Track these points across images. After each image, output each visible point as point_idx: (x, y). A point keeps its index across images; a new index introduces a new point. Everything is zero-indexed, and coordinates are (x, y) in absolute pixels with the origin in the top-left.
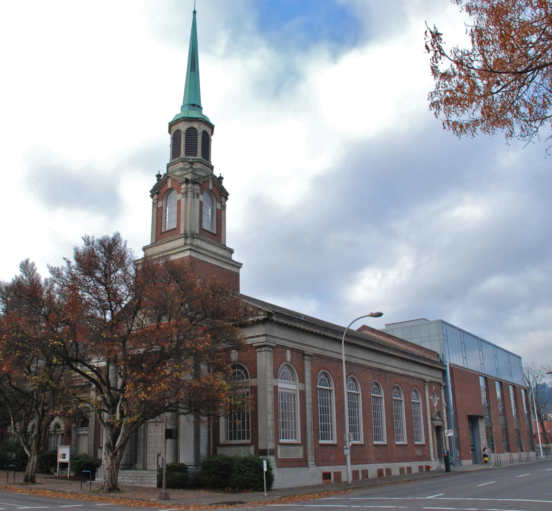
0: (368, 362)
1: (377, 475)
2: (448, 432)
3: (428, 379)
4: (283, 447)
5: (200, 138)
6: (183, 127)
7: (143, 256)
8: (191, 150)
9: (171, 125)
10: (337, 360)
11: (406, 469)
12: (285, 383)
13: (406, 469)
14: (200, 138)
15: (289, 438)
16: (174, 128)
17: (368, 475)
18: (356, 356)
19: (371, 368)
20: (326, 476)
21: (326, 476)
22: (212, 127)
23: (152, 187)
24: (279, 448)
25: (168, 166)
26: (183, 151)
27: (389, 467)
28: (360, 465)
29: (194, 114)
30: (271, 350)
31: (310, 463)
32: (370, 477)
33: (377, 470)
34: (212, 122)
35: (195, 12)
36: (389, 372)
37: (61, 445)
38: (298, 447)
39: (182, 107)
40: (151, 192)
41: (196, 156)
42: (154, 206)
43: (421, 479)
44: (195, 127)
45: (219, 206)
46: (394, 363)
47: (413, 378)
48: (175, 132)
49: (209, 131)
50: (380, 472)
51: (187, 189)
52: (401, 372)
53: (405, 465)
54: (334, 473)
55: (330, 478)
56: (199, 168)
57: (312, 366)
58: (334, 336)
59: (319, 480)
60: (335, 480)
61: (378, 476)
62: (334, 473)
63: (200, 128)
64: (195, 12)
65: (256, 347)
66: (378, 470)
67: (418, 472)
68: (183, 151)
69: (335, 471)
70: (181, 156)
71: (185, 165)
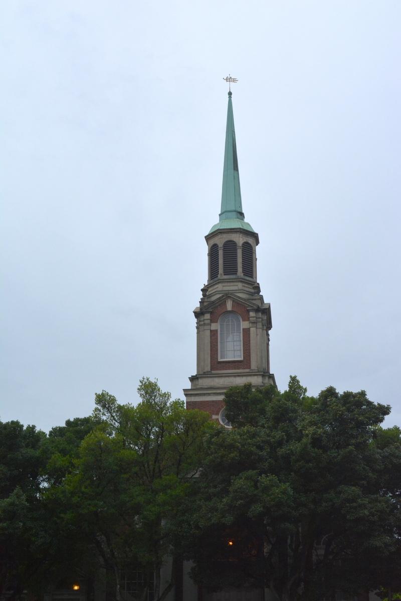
6: (220, 241)
7: (195, 375)
8: (230, 268)
9: (208, 238)
16: (212, 242)
22: (255, 236)
23: (83, 417)
26: (221, 271)
29: (235, 224)
34: (256, 231)
35: (230, 94)
37: (252, 277)
39: (220, 215)
40: (363, 394)
41: (236, 274)
42: (202, 328)
44: (249, 242)
45: (265, 318)
48: (212, 247)
49: (251, 241)
56: (240, 288)
63: (240, 240)
64: (230, 94)
68: (221, 271)
70: (219, 276)
71: (223, 286)
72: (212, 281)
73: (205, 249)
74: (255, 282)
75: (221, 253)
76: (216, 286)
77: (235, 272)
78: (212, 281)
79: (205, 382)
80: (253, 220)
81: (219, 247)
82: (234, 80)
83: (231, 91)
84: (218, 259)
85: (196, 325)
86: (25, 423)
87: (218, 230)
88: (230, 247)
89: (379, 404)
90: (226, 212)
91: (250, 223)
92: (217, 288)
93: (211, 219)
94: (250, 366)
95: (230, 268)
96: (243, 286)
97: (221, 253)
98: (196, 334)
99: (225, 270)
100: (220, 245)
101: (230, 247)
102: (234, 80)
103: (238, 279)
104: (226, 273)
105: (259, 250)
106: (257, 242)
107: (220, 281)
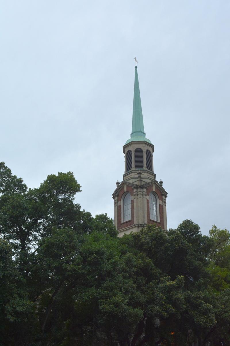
5: (145, 155)
6: (133, 148)
8: (139, 165)
9: (125, 147)
14: (145, 155)
22: (152, 147)
25: (124, 176)
35: (136, 67)
39: (131, 134)
41: (143, 168)
48: (127, 152)
49: (150, 149)
63: (145, 148)
64: (136, 67)
72: (127, 172)
73: (122, 157)
74: (153, 173)
75: (133, 156)
76: (131, 175)
77: (142, 167)
78: (127, 172)
79: (128, 177)
80: (150, 136)
81: (132, 151)
83: (137, 66)
84: (132, 165)
85: (112, 196)
86: (181, 222)
87: (132, 142)
88: (139, 152)
90: (135, 132)
91: (149, 139)
92: (131, 175)
93: (127, 138)
95: (139, 165)
96: (147, 175)
97: (133, 156)
98: (114, 209)
99: (136, 167)
101: (139, 152)
103: (143, 171)
104: (136, 167)
107: (133, 171)
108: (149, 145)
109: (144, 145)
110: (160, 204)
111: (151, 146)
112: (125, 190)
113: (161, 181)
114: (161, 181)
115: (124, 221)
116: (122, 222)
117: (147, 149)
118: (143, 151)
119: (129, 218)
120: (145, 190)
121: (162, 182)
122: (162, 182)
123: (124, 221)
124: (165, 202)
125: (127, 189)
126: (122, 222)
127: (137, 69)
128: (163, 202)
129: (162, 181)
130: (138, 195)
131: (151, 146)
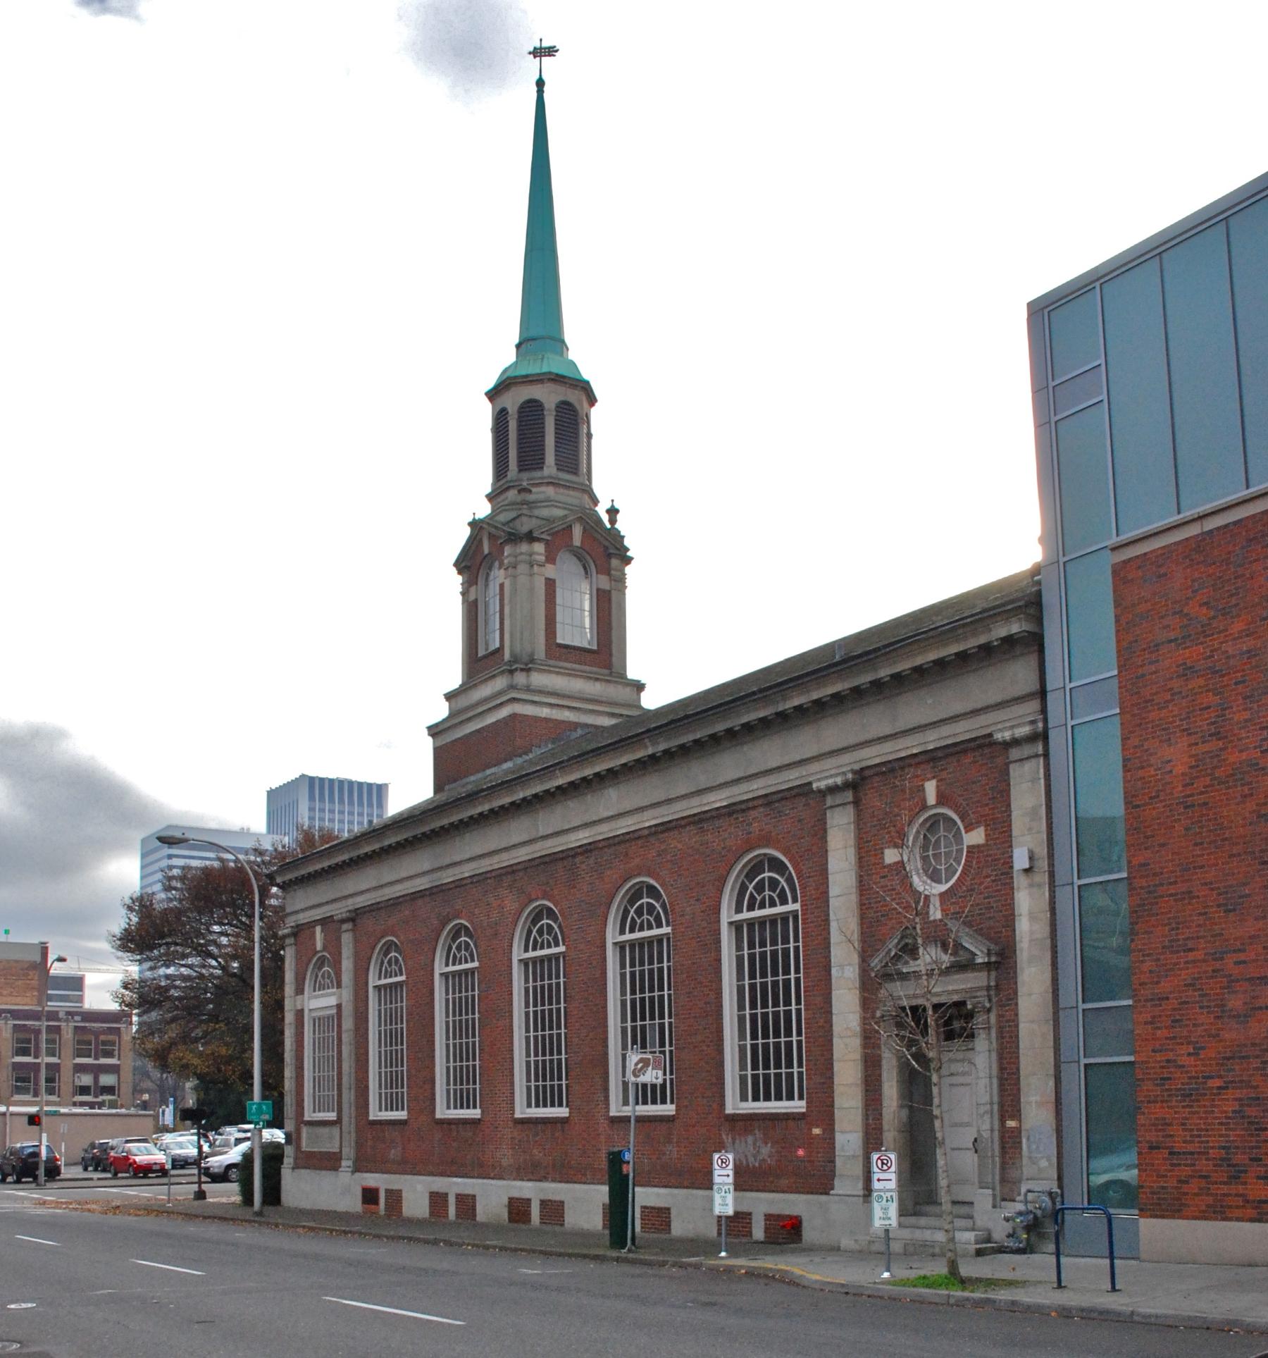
0: (496, 859)
1: (505, 1215)
2: (646, 1063)
3: (826, 775)
4: (311, 1129)
6: (512, 401)
8: (531, 458)
9: (492, 395)
10: (408, 898)
11: (452, 1200)
12: (322, 996)
13: (452, 1200)
15: (654, 1102)
17: (474, 1210)
18: (347, 893)
19: (511, 870)
20: (370, 1196)
21: (370, 1196)
24: (305, 1131)
27: (558, 1198)
28: (459, 1180)
30: (849, 796)
31: (344, 1163)
32: (481, 1216)
33: (506, 1201)
34: (586, 375)
35: (540, 84)
36: (587, 850)
38: (324, 1131)
39: (518, 346)
40: (623, 537)
43: (541, 1252)
46: (611, 800)
47: (732, 810)
49: (573, 396)
50: (518, 1210)
51: (516, 557)
52: (649, 820)
53: (455, 1185)
54: (387, 1191)
55: (376, 1202)
57: (356, 941)
58: (376, 846)
59: (354, 1203)
60: (386, 1209)
61: (511, 1220)
62: (387, 1191)
63: (549, 397)
64: (540, 84)
65: (823, 793)
66: (511, 1200)
67: (427, 1215)
69: (390, 1187)
73: (485, 413)
82: (550, 51)
88: (531, 410)
89: (854, 772)
94: (670, 1230)
99: (319, 1019)
100: (513, 410)
102: (550, 51)
105: (599, 418)
106: (592, 400)
108: (524, 382)
109: (550, 386)
110: (602, 587)
111: (531, 381)
112: (486, 551)
113: (613, 506)
114: (613, 506)
115: (487, 649)
116: (481, 653)
117: (563, 398)
118: (546, 406)
119: (497, 645)
120: (539, 548)
121: (617, 511)
122: (617, 511)
123: (487, 649)
124: (620, 581)
125: (489, 548)
126: (481, 653)
127: (545, 89)
128: (611, 580)
129: (617, 506)
130: (519, 567)
131: (531, 381)
